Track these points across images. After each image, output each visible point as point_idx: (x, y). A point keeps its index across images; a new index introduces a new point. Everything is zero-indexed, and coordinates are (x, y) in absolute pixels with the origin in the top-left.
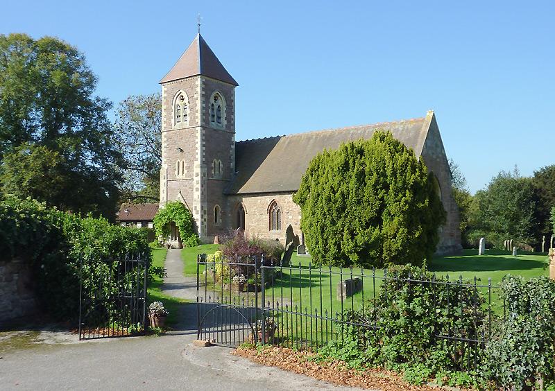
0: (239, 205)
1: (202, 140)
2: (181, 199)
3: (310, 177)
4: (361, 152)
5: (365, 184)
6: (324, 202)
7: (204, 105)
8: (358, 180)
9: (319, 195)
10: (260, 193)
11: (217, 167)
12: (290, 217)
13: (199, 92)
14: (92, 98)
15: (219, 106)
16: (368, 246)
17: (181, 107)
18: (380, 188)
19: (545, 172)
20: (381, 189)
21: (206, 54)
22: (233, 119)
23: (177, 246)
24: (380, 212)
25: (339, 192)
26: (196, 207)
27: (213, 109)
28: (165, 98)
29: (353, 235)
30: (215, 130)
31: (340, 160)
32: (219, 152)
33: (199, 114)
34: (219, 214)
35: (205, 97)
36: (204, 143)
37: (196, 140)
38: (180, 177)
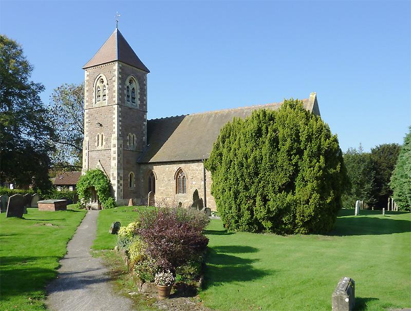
0: (150, 172)
1: (119, 116)
2: (100, 166)
3: (221, 145)
4: (272, 118)
5: (279, 150)
6: (236, 168)
7: (120, 86)
8: (272, 145)
9: (231, 161)
10: (169, 162)
11: (132, 139)
12: (194, 183)
13: (117, 76)
14: (29, 82)
15: (133, 89)
16: (282, 212)
17: (101, 89)
18: (294, 154)
19: (379, 150)
20: (295, 154)
21: (122, 44)
22: (146, 100)
23: (97, 208)
24: (293, 177)
25: (252, 157)
26: (113, 174)
27: (128, 91)
28: (87, 81)
29: (265, 200)
30: (130, 108)
31: (253, 126)
32: (133, 127)
33: (116, 94)
34: (133, 180)
35: (122, 80)
36: (120, 123)
37: (114, 116)
38: (100, 147)
